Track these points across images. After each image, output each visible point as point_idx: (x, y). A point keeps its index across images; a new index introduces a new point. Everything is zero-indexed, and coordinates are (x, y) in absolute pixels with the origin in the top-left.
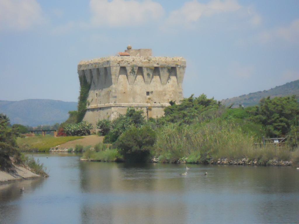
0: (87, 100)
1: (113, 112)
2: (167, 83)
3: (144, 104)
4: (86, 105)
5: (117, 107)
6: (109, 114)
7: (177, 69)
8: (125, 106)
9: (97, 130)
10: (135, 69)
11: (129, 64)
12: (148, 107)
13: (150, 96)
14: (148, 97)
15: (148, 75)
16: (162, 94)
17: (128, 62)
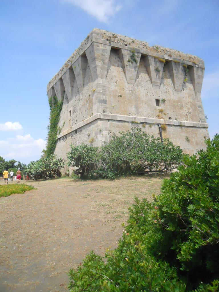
0: (58, 127)
1: (101, 131)
2: (183, 90)
3: (154, 119)
4: (56, 134)
5: (109, 120)
6: (93, 136)
7: (195, 69)
8: (122, 120)
9: (73, 169)
10: (137, 57)
11: (126, 45)
12: (160, 124)
13: (162, 107)
14: (159, 108)
15: (157, 70)
16: (177, 106)
17: (124, 41)
